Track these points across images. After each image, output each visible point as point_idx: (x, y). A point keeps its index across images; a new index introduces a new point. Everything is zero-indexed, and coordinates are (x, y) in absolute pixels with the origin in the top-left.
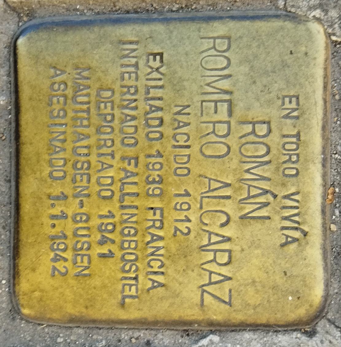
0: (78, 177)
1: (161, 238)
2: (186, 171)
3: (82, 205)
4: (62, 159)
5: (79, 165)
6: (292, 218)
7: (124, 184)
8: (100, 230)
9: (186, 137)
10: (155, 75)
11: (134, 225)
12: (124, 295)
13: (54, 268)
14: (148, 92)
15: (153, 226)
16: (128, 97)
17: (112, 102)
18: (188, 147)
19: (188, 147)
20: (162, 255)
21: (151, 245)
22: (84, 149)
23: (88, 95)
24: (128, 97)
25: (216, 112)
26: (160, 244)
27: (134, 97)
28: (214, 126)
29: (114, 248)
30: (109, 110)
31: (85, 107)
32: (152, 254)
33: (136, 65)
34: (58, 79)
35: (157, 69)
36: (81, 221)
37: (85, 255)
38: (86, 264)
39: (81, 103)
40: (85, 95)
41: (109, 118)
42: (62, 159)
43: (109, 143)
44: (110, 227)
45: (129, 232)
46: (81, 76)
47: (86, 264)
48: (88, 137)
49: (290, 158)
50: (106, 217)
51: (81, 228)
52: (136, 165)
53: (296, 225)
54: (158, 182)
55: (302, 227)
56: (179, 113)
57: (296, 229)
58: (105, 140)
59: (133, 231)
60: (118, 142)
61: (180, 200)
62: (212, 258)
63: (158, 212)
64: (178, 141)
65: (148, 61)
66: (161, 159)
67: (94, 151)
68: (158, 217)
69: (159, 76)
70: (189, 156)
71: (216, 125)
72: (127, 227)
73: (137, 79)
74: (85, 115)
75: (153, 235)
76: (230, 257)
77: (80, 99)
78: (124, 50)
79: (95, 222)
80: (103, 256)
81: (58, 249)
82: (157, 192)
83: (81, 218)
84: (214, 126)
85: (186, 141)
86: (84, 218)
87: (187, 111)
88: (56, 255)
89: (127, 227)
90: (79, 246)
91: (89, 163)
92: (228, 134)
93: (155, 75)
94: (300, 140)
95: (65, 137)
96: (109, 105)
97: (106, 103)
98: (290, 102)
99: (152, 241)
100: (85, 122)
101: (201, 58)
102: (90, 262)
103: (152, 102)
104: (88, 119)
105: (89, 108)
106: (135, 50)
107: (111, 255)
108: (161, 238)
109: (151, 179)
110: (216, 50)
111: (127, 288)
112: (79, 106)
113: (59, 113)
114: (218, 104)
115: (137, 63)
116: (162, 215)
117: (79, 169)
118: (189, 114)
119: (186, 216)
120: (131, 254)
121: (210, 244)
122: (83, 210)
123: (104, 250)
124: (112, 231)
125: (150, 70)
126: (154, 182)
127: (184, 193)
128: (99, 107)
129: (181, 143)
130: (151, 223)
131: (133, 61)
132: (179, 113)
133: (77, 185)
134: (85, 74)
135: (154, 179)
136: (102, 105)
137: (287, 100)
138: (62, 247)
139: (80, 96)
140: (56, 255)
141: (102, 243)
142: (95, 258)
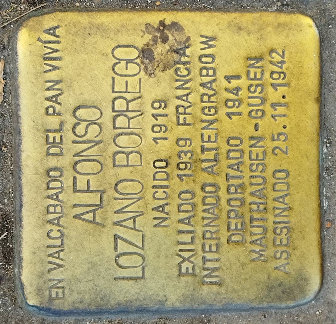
0: (261, 157)
1: (178, 98)
2: (158, 164)
3: (256, 127)
4: (278, 191)
5: (260, 168)
6: (51, 68)
7: (215, 160)
8: (240, 101)
9: (157, 195)
10: (186, 255)
11: (205, 117)
12: (214, 77)
13: (283, 57)
14: (193, 238)
15: (185, 108)
16: (213, 229)
17: (229, 229)
18: (154, 187)
19: (154, 187)
20: (177, 80)
21: (187, 91)
22: (257, 232)
23: (252, 234)
24: (213, 229)
25: (127, 69)
26: (180, 92)
27: (207, 228)
28: (128, 108)
29: (225, 84)
30: (233, 222)
31: (255, 223)
32: (186, 82)
33: (205, 260)
34: (283, 261)
35: (185, 260)
36: (257, 111)
37: (252, 79)
38: (252, 70)
39: (258, 226)
40: (255, 234)
41: (232, 215)
42: (278, 191)
43: (233, 189)
44: (230, 104)
45: (209, 111)
46: (259, 254)
47: (252, 70)
48: (252, 194)
49: (185, 110)
50: (234, 114)
51: (255, 105)
52: (202, 135)
53: (46, 45)
54: (182, 152)
55: (41, 44)
56: (164, 219)
57: (46, 42)
58: (236, 192)
59: (206, 111)
60: (223, 189)
61: (160, 111)
62: (131, 120)
63: (181, 121)
64: (164, 192)
65: (194, 268)
66: (179, 173)
67: (246, 180)
68: (182, 117)
69: (181, 253)
70: (154, 179)
71: (125, 163)
72: (210, 115)
73: (203, 246)
74: (255, 216)
75: (187, 101)
76: (114, 160)
77: (259, 230)
78: (217, 276)
79: (244, 109)
80: (238, 77)
81: (279, 73)
82: (182, 143)
83: (257, 114)
84: (128, 108)
85: (157, 192)
86: (253, 114)
87: (156, 222)
88: (281, 67)
89: (210, 115)
90: (259, 89)
91: (251, 171)
92: (114, 100)
93: (186, 255)
94: (49, 273)
95: (274, 212)
96: (233, 227)
97: (236, 229)
98: (54, 138)
99: (187, 95)
100: (254, 207)
101: (141, 193)
102: (248, 73)
103: (190, 228)
104: (251, 210)
105: (251, 222)
106: (206, 225)
107: (228, 78)
108: (178, 98)
109: (189, 155)
110: (125, 99)
111: (213, 139)
112: (262, 224)
113: (281, 231)
114: (125, 91)
115: (204, 263)
116: (178, 118)
117: (261, 164)
118: (155, 218)
119: (157, 143)
120: (232, 146)
121: (134, 218)
122: (254, 122)
123: (235, 83)
124: (228, 100)
125: (192, 259)
126: (186, 153)
127: (158, 141)
128: (242, 225)
129: (161, 191)
130: (188, 111)
131: (209, 265)
132: (164, 219)
133: (260, 70)
134: (255, 256)
135: (186, 155)
136: (239, 227)
137: (58, 140)
138: (275, 76)
139: (260, 234)
140: (281, 67)
141: (238, 89)
142: (244, 77)
